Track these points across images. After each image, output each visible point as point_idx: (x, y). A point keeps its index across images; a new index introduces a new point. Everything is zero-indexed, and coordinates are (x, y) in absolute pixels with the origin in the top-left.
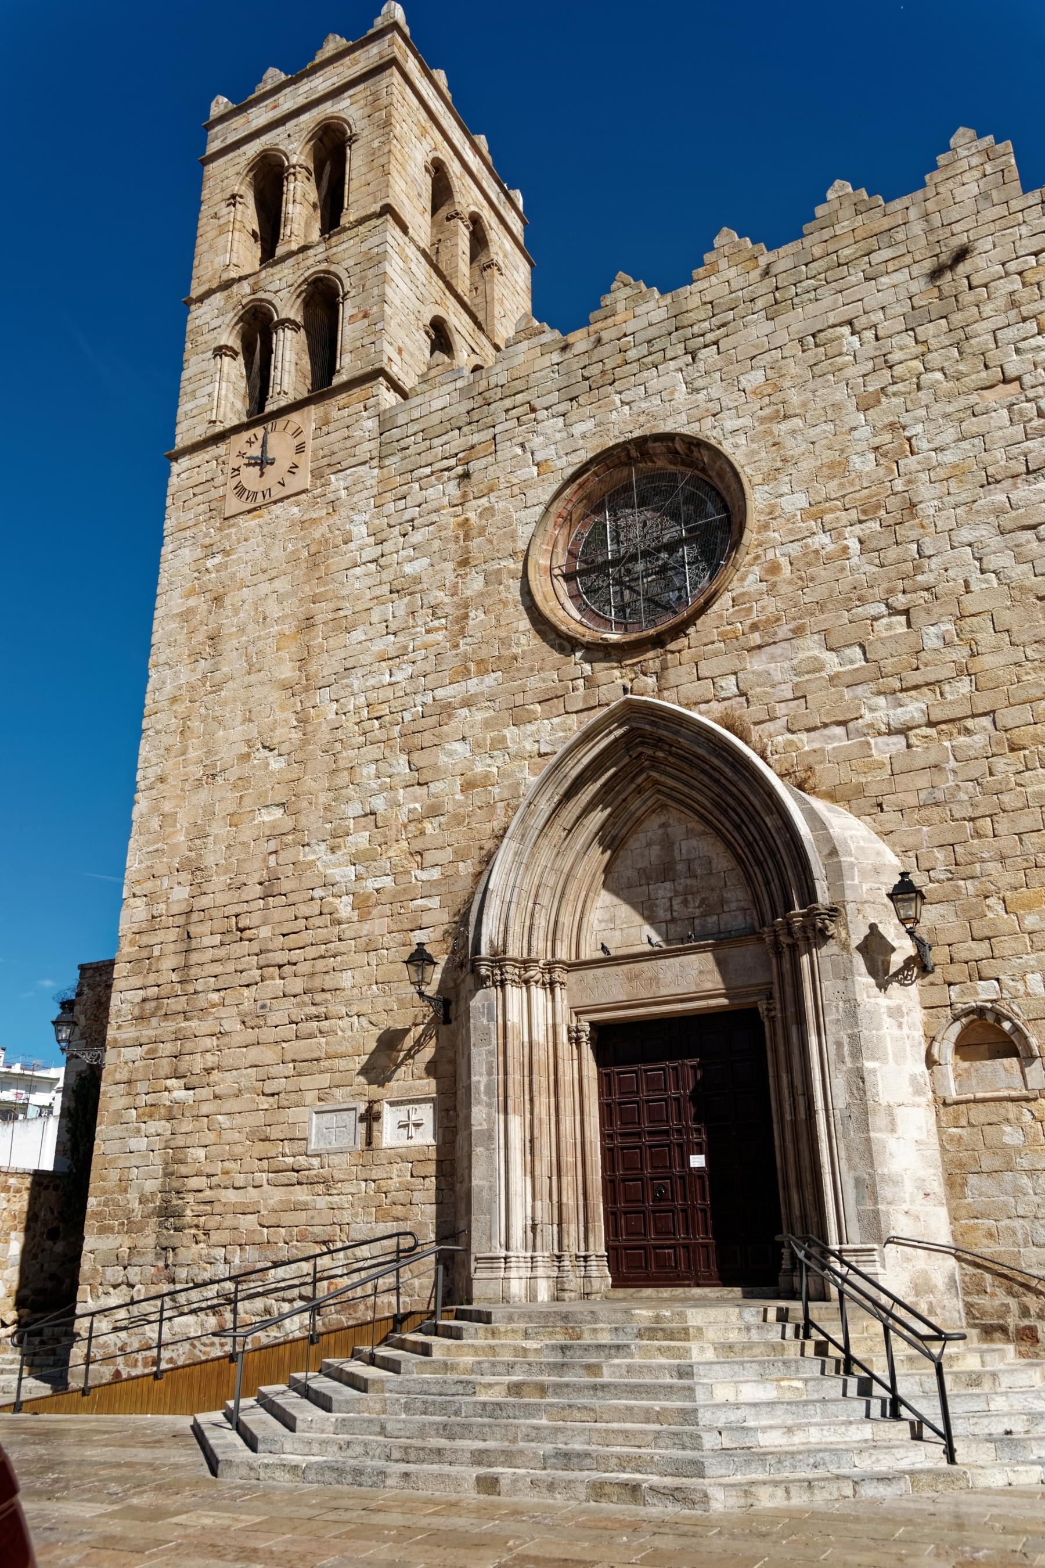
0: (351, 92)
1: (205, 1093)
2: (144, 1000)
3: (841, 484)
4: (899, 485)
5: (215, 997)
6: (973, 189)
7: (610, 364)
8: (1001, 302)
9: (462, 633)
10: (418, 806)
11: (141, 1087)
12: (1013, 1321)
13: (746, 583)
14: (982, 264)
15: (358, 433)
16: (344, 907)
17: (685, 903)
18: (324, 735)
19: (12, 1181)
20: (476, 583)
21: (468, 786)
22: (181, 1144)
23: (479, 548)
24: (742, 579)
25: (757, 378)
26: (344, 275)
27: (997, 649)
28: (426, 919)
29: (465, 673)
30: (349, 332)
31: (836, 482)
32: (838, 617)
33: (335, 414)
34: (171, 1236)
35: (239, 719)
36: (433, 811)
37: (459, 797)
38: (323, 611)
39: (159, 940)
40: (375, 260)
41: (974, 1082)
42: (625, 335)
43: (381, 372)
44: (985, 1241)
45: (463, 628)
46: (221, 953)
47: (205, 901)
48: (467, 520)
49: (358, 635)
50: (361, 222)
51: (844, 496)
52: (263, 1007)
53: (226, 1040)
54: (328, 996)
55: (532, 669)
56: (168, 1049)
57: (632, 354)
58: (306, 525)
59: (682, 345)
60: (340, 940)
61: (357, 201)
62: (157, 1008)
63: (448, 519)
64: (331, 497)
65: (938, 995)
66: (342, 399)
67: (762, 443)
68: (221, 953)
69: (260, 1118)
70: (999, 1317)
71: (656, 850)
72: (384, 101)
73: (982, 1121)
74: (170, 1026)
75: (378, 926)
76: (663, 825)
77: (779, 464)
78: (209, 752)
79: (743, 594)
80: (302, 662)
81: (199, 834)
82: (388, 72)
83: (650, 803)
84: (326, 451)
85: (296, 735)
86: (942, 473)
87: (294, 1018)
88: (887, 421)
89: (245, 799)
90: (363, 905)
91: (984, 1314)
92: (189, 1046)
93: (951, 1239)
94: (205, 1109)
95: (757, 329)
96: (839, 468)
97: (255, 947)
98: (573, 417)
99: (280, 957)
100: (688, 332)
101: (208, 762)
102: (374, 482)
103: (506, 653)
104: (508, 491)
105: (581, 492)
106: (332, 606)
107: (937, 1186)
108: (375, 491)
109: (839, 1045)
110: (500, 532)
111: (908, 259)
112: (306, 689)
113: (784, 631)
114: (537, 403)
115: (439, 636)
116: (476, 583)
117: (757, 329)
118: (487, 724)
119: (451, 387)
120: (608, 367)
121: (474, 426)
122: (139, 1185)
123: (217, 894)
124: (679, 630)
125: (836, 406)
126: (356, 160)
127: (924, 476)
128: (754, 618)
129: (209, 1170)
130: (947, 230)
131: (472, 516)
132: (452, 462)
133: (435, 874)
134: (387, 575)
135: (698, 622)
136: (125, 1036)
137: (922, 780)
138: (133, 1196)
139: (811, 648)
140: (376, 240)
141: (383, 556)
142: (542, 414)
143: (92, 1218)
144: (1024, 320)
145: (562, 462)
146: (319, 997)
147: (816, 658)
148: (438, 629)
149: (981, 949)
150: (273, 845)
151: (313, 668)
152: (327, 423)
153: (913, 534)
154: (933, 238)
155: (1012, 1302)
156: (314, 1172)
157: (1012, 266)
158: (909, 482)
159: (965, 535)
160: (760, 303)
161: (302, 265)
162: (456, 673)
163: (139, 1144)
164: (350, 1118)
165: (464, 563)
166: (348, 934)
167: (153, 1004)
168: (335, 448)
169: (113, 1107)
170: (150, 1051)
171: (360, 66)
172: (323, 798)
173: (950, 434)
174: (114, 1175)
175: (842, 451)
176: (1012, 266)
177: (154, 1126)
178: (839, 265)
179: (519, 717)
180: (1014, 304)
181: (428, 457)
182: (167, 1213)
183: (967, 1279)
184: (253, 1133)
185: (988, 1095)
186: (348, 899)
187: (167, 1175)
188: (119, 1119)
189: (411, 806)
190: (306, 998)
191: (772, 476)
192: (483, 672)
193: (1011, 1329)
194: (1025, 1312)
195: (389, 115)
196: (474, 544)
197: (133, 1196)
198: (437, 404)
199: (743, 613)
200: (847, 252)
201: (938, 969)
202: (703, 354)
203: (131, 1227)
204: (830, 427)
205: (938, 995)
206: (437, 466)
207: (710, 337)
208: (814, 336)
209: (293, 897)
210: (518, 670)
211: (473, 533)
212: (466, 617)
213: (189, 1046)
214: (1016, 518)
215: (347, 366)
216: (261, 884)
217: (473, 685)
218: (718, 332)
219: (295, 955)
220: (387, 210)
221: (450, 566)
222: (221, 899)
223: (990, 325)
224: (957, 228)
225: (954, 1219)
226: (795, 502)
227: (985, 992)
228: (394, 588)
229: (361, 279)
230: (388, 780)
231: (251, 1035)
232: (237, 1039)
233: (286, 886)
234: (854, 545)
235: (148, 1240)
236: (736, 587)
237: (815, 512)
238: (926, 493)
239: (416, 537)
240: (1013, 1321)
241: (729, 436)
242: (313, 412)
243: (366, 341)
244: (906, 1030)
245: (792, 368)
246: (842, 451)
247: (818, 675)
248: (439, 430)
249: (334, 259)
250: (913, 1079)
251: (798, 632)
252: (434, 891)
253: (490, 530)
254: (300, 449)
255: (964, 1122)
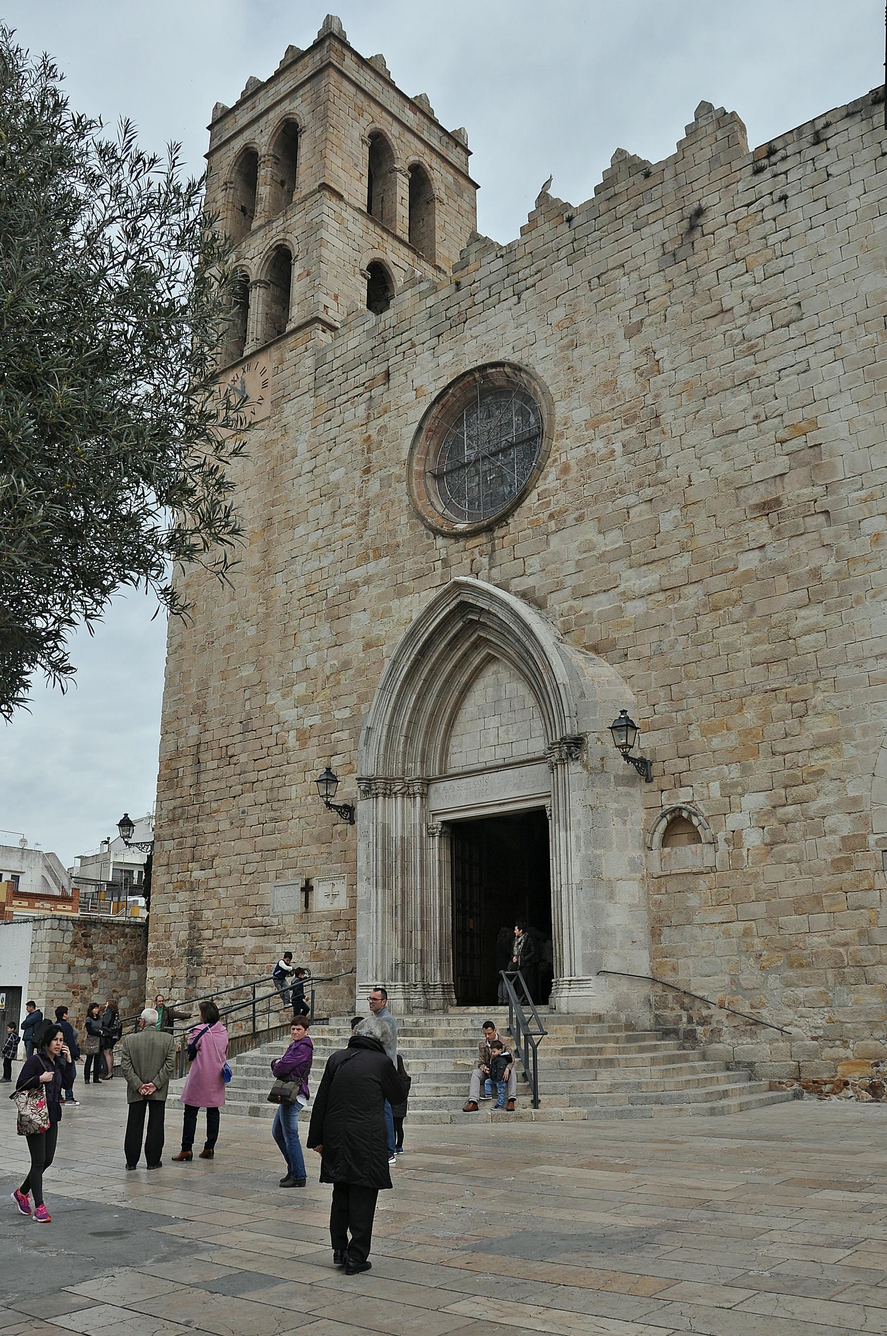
0: (301, 92)
1: (210, 873)
2: (174, 808)
3: (612, 399)
4: (649, 400)
5: (214, 805)
6: (708, 153)
7: (464, 305)
8: (722, 247)
9: (365, 526)
10: (336, 662)
11: (176, 868)
12: (683, 1025)
13: (548, 482)
14: (711, 221)
15: (302, 370)
16: (292, 739)
17: (507, 732)
18: (278, 609)
19: (127, 930)
20: (374, 487)
21: (368, 646)
22: (198, 907)
23: (376, 458)
24: (545, 479)
25: (558, 314)
26: (294, 241)
27: (707, 532)
28: (339, 748)
29: (365, 558)
30: (298, 288)
31: (608, 397)
32: (606, 508)
33: (288, 355)
34: (195, 969)
35: (227, 599)
36: (346, 666)
37: (362, 655)
38: (278, 513)
39: (182, 765)
40: (314, 228)
41: (673, 861)
42: (474, 282)
43: (317, 320)
44: (671, 973)
45: (366, 522)
46: (218, 773)
47: (208, 736)
48: (370, 436)
49: (300, 531)
50: (305, 199)
51: (613, 409)
52: (243, 812)
53: (221, 836)
54: (281, 804)
55: (409, 555)
56: (190, 841)
57: (479, 298)
58: (268, 445)
59: (511, 288)
60: (288, 763)
61: (306, 181)
62: (182, 814)
63: (357, 436)
64: (284, 422)
65: (655, 799)
66: (291, 340)
67: (561, 367)
68: (218, 773)
69: (241, 891)
70: (675, 1024)
71: (490, 691)
72: (324, 97)
73: (675, 890)
74: (190, 826)
75: (312, 750)
76: (495, 673)
77: (572, 384)
78: (209, 624)
79: (545, 490)
80: (265, 553)
81: (204, 686)
82: (326, 73)
83: (566, 340)
84: (280, 386)
85: (262, 610)
86: (677, 388)
87: (261, 821)
88: (644, 347)
89: (231, 659)
90: (303, 737)
91: (666, 1021)
92: (201, 840)
93: (650, 973)
94: (212, 884)
95: (561, 272)
96: (611, 385)
97: (238, 770)
98: (439, 350)
99: (252, 777)
100: (514, 278)
101: (209, 632)
102: (311, 409)
103: (393, 542)
104: (395, 412)
105: (444, 410)
106: (284, 508)
107: (642, 936)
108: (311, 416)
109: (578, 838)
110: (391, 445)
111: (662, 213)
112: (268, 573)
113: (570, 519)
114: (416, 340)
115: (349, 530)
116: (374, 487)
117: (561, 272)
118: (380, 598)
119: (361, 329)
120: (463, 308)
121: (375, 361)
122: (175, 935)
123: (215, 732)
124: (502, 519)
125: (611, 336)
126: (305, 146)
127: (666, 392)
128: (553, 508)
129: (214, 926)
130: (689, 187)
131: (373, 433)
132: (361, 390)
133: (347, 713)
134: (319, 483)
135: (516, 514)
136: (164, 833)
137: (654, 636)
138: (173, 942)
139: (588, 531)
140: (315, 212)
141: (316, 467)
142: (418, 349)
143: (150, 956)
144: (737, 261)
145: (431, 388)
146: (276, 805)
147: (590, 541)
148: (351, 524)
149: (682, 764)
150: (247, 694)
151: (271, 558)
152: (282, 363)
153: (657, 440)
154: (680, 195)
155: (684, 1014)
156: (275, 927)
157: (731, 217)
158: (657, 396)
159: (689, 440)
160: (563, 253)
161: (268, 236)
162: (361, 558)
163: (174, 907)
164: (298, 889)
165: (367, 471)
166: (293, 759)
167: (180, 810)
168: (286, 382)
169: (159, 883)
170: (180, 844)
171: (309, 69)
172: (279, 657)
173: (685, 356)
174: (161, 928)
175: (614, 372)
176: (731, 217)
177: (183, 896)
178: (617, 219)
179: (400, 591)
180: (731, 249)
181: (345, 387)
182: (193, 953)
183: (657, 999)
184: (239, 900)
185: (679, 871)
186: (293, 733)
187: (192, 928)
188: (163, 891)
189: (332, 663)
190: (269, 806)
191: (567, 394)
192: (378, 557)
193: (682, 1031)
194: (690, 1020)
195: (327, 109)
196: (373, 456)
197: (173, 942)
198: (352, 344)
199: (544, 506)
200: (622, 208)
201: (655, 780)
202: (525, 295)
203: (172, 963)
204: (605, 353)
205: (655, 799)
206: (351, 394)
207: (530, 281)
208: (598, 277)
209: (261, 733)
210: (399, 555)
211: (374, 446)
212: (367, 514)
213: (201, 840)
214: (724, 424)
215: (297, 316)
216: (241, 722)
217: (372, 568)
218: (536, 277)
219: (262, 775)
220: (324, 187)
221: (358, 473)
222: (218, 734)
223: (715, 265)
224: (696, 186)
225: (653, 958)
226: (581, 414)
227: (683, 796)
228: (323, 493)
229: (305, 245)
230: (317, 643)
231: (236, 833)
232: (229, 835)
233: (256, 724)
234: (618, 447)
235: (182, 971)
236: (541, 486)
237: (594, 424)
238: (667, 405)
239: (337, 451)
240: (683, 1025)
241: (540, 362)
242: (274, 353)
243: (309, 294)
244: (629, 826)
245: (584, 306)
246: (614, 372)
247: (592, 553)
248: (353, 364)
249: (290, 229)
250: (632, 861)
251: (580, 519)
252: (345, 727)
253: (384, 444)
254: (265, 384)
255: (664, 892)
